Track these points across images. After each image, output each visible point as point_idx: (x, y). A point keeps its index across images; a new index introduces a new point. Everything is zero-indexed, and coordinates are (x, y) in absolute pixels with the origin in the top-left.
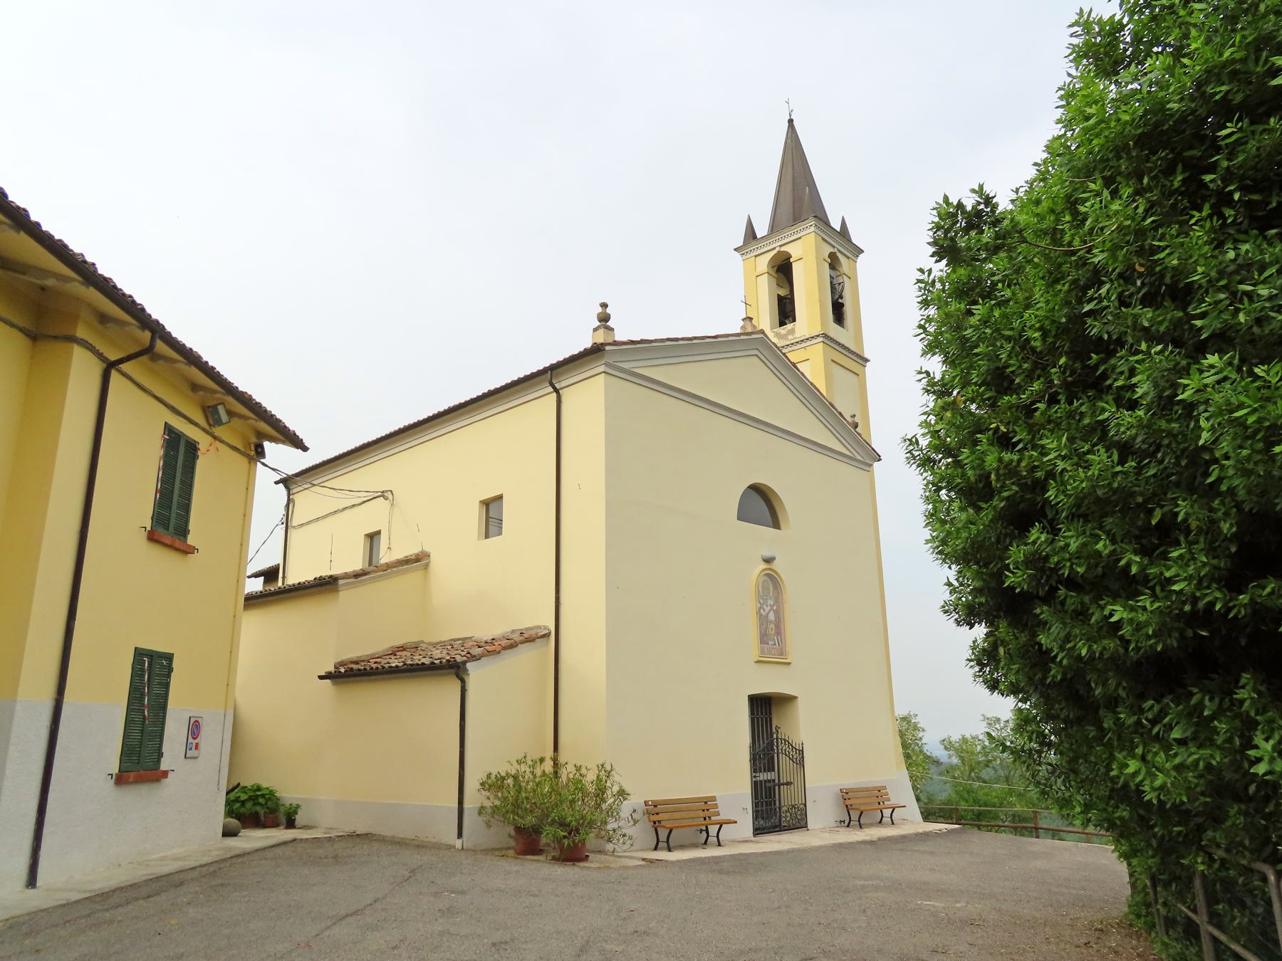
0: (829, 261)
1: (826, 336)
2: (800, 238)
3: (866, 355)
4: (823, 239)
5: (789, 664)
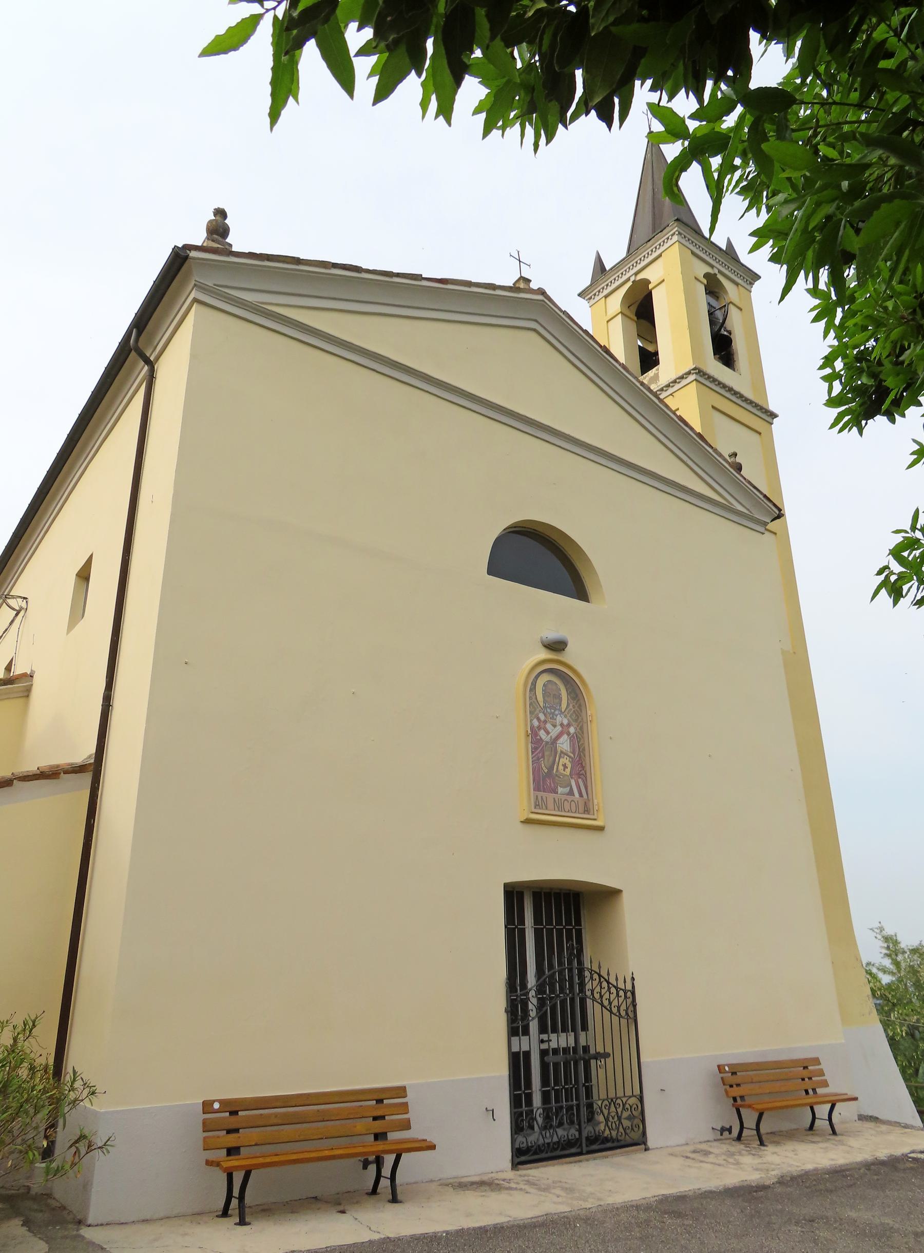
0: (705, 281)
1: (699, 372)
2: (660, 256)
3: (772, 407)
4: (693, 253)
5: (601, 829)
